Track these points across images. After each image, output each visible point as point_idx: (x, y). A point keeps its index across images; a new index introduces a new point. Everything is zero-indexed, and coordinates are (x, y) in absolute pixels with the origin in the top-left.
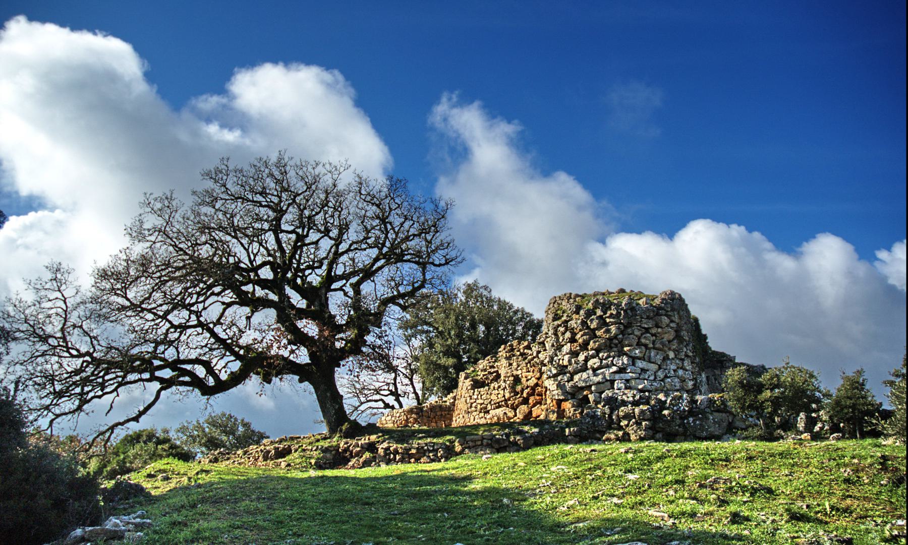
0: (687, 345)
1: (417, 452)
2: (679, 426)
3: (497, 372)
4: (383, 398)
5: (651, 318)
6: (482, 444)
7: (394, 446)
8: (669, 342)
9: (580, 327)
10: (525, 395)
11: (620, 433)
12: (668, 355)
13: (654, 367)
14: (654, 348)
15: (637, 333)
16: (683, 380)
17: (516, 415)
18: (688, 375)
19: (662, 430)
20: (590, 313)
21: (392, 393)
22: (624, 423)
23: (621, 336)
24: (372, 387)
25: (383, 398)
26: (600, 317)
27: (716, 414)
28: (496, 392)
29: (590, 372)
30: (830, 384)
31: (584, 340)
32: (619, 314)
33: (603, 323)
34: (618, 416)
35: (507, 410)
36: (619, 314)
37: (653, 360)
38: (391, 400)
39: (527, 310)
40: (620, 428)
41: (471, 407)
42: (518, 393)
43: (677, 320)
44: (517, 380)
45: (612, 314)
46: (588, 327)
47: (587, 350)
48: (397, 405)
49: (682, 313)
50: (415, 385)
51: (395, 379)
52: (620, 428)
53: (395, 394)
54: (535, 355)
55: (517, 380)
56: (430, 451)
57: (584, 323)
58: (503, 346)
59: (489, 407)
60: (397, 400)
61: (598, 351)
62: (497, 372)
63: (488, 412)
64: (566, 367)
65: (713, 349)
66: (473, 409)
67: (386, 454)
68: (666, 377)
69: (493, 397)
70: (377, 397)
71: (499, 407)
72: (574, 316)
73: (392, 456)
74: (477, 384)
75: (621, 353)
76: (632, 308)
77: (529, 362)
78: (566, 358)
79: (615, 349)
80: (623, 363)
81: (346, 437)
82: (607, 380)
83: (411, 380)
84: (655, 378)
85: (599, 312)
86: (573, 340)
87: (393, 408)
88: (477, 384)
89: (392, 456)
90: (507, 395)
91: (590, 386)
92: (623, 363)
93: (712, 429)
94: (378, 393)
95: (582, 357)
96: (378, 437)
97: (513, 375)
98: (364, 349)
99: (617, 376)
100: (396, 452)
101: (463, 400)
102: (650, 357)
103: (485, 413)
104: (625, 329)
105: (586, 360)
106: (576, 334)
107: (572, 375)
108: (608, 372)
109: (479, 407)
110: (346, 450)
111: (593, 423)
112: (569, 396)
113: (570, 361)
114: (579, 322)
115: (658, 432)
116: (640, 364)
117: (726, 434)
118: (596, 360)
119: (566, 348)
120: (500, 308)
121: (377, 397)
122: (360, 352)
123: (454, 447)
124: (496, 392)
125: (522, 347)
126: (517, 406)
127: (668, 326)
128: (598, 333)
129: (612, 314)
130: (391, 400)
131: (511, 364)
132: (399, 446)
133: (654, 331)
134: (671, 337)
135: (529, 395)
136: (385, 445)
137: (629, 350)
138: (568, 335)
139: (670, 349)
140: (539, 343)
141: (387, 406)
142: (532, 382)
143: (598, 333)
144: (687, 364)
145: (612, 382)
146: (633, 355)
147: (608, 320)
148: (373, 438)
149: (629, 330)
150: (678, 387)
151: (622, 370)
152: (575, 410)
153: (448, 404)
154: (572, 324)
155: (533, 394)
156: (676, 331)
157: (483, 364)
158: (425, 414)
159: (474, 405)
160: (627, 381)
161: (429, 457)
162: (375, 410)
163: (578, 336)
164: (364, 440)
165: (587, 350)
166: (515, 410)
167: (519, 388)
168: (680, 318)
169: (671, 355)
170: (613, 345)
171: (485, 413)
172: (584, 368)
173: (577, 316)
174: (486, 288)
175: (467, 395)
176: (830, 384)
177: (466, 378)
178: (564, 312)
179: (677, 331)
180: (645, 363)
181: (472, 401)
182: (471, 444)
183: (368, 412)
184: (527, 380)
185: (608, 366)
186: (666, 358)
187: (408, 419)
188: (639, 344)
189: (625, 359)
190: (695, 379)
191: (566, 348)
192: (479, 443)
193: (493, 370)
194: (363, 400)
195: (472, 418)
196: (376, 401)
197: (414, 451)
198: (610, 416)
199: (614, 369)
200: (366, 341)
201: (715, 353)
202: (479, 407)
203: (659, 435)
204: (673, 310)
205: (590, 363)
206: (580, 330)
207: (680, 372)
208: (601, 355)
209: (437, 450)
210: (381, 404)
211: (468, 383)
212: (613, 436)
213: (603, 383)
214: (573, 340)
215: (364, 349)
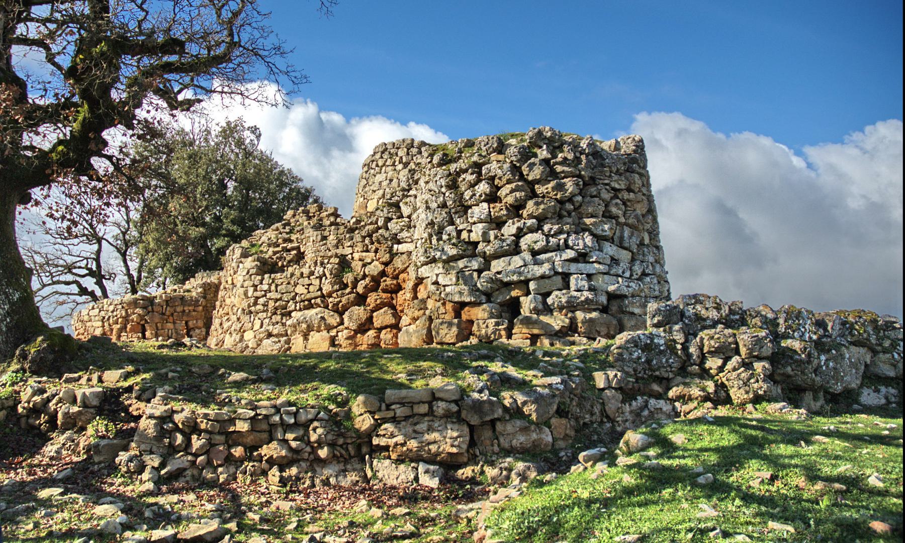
1: (252, 430)
4: (78, 279)
6: (431, 413)
7: (184, 411)
8: (643, 216)
9: (509, 176)
10: (360, 289)
11: (710, 387)
13: (625, 256)
15: (606, 196)
17: (342, 323)
21: (91, 273)
22: (713, 363)
23: (579, 198)
24: (61, 262)
25: (78, 279)
26: (546, 162)
27: (853, 349)
29: (527, 256)
31: (516, 200)
33: (551, 174)
34: (701, 348)
35: (327, 314)
36: (577, 160)
37: (626, 245)
38: (90, 283)
40: (705, 374)
41: (255, 304)
42: (346, 286)
44: (344, 264)
45: (565, 159)
46: (522, 177)
47: (520, 216)
48: (98, 293)
50: (129, 263)
51: (99, 252)
52: (705, 374)
53: (98, 275)
54: (380, 223)
55: (344, 264)
56: (287, 428)
57: (515, 169)
60: (99, 283)
61: (541, 220)
62: (298, 248)
63: (289, 314)
64: (476, 244)
66: (259, 307)
67: (162, 433)
69: (300, 289)
70: (69, 277)
71: (310, 306)
72: (494, 156)
73: (179, 438)
74: (267, 267)
75: (580, 229)
77: (370, 236)
78: (478, 229)
79: (570, 220)
80: (585, 245)
81: (36, 372)
82: (556, 273)
83: (124, 255)
84: (631, 275)
85: (543, 153)
86: (492, 198)
87: (92, 294)
88: (267, 267)
89: (179, 438)
90: (327, 288)
91: (526, 282)
92: (585, 245)
94: (70, 272)
95: (510, 229)
96: (127, 376)
98: (96, 162)
99: (573, 267)
100: (192, 428)
102: (622, 238)
103: (283, 315)
104: (587, 184)
105: (520, 234)
106: (498, 188)
107: (488, 260)
108: (559, 259)
109: (271, 304)
110: (36, 411)
111: (648, 361)
112: (484, 298)
113: (485, 234)
114: (506, 166)
116: (610, 249)
118: (537, 236)
119: (480, 211)
121: (69, 277)
122: (86, 169)
123: (349, 416)
124: (306, 281)
126: (345, 308)
128: (540, 189)
129: (565, 159)
130: (90, 283)
131: (324, 238)
132: (201, 411)
133: (626, 195)
135: (369, 290)
136: (156, 407)
137: (594, 224)
138: (483, 188)
141: (83, 291)
142: (375, 268)
143: (540, 189)
145: (566, 276)
146: (599, 232)
147: (559, 168)
148: (112, 377)
149: (593, 190)
151: (582, 257)
152: (497, 324)
153: (194, 294)
154: (493, 167)
155: (375, 289)
158: (156, 308)
159: (261, 301)
160: (590, 277)
161: (285, 441)
162: (64, 297)
163: (502, 193)
164: (86, 386)
165: (520, 216)
166: (341, 314)
167: (348, 278)
170: (564, 211)
171: (283, 315)
172: (515, 250)
173: (501, 157)
174: (254, 130)
181: (258, 294)
182: (400, 411)
183: (52, 299)
184: (364, 265)
185: (558, 248)
187: (128, 315)
188: (608, 216)
189: (588, 240)
191: (480, 211)
192: (424, 409)
193: (290, 246)
194: (46, 280)
196: (67, 283)
197: (242, 426)
198: (685, 348)
199: (570, 254)
200: (105, 143)
202: (271, 304)
205: (525, 242)
206: (509, 182)
208: (546, 228)
209: (306, 425)
210: (74, 289)
212: (696, 392)
213: (549, 277)
214: (492, 198)
215: (96, 162)
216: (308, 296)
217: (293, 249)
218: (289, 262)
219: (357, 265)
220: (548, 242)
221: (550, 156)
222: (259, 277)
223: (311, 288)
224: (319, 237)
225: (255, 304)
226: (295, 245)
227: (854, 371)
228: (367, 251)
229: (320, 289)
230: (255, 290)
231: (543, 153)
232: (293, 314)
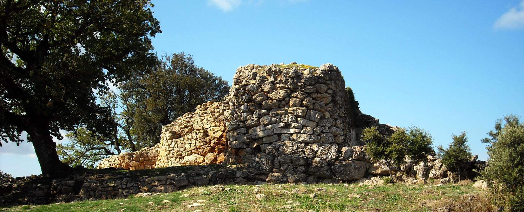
0: (341, 108)
2: (327, 171)
3: (192, 125)
5: (313, 85)
8: (326, 105)
10: (212, 144)
12: (324, 115)
14: (314, 109)
16: (336, 136)
18: (340, 131)
19: (313, 174)
20: (264, 80)
26: (273, 82)
28: (189, 142)
30: (441, 142)
32: (286, 81)
39: (223, 79)
41: (169, 153)
42: (207, 143)
43: (333, 88)
48: (116, 152)
49: (337, 82)
54: (221, 112)
55: (205, 131)
58: (199, 106)
59: (184, 154)
62: (192, 125)
63: (183, 158)
65: (363, 113)
66: (171, 155)
68: (322, 132)
69: (187, 146)
71: (191, 154)
74: (175, 136)
76: (298, 75)
87: (113, 154)
88: (175, 136)
90: (198, 144)
92: (288, 120)
93: (353, 174)
97: (203, 129)
101: (164, 147)
103: (180, 158)
109: (176, 153)
115: (310, 175)
117: (363, 178)
120: (202, 76)
125: (213, 107)
127: (326, 92)
129: (281, 81)
133: (314, 96)
134: (328, 102)
139: (326, 110)
140: (225, 103)
144: (339, 122)
150: (331, 141)
156: (332, 96)
157: (181, 120)
168: (336, 86)
169: (327, 115)
175: (167, 144)
176: (441, 142)
177: (166, 130)
178: (243, 79)
179: (333, 96)
180: (306, 121)
186: (323, 117)
190: (345, 135)
195: (170, 162)
201: (364, 116)
203: (311, 178)
204: (330, 80)
207: (334, 129)
208: (271, 114)
211: (168, 134)
216: (191, 149)
217: (189, 126)
218: (187, 132)
219: (210, 133)
220: (271, 119)
221: (274, 80)
222: (171, 141)
223: (192, 145)
224: (200, 120)
225: (169, 153)
226: (190, 124)
227: (357, 171)
228: (216, 126)
229: (195, 145)
230: (169, 147)
231: (271, 79)
232: (184, 158)
